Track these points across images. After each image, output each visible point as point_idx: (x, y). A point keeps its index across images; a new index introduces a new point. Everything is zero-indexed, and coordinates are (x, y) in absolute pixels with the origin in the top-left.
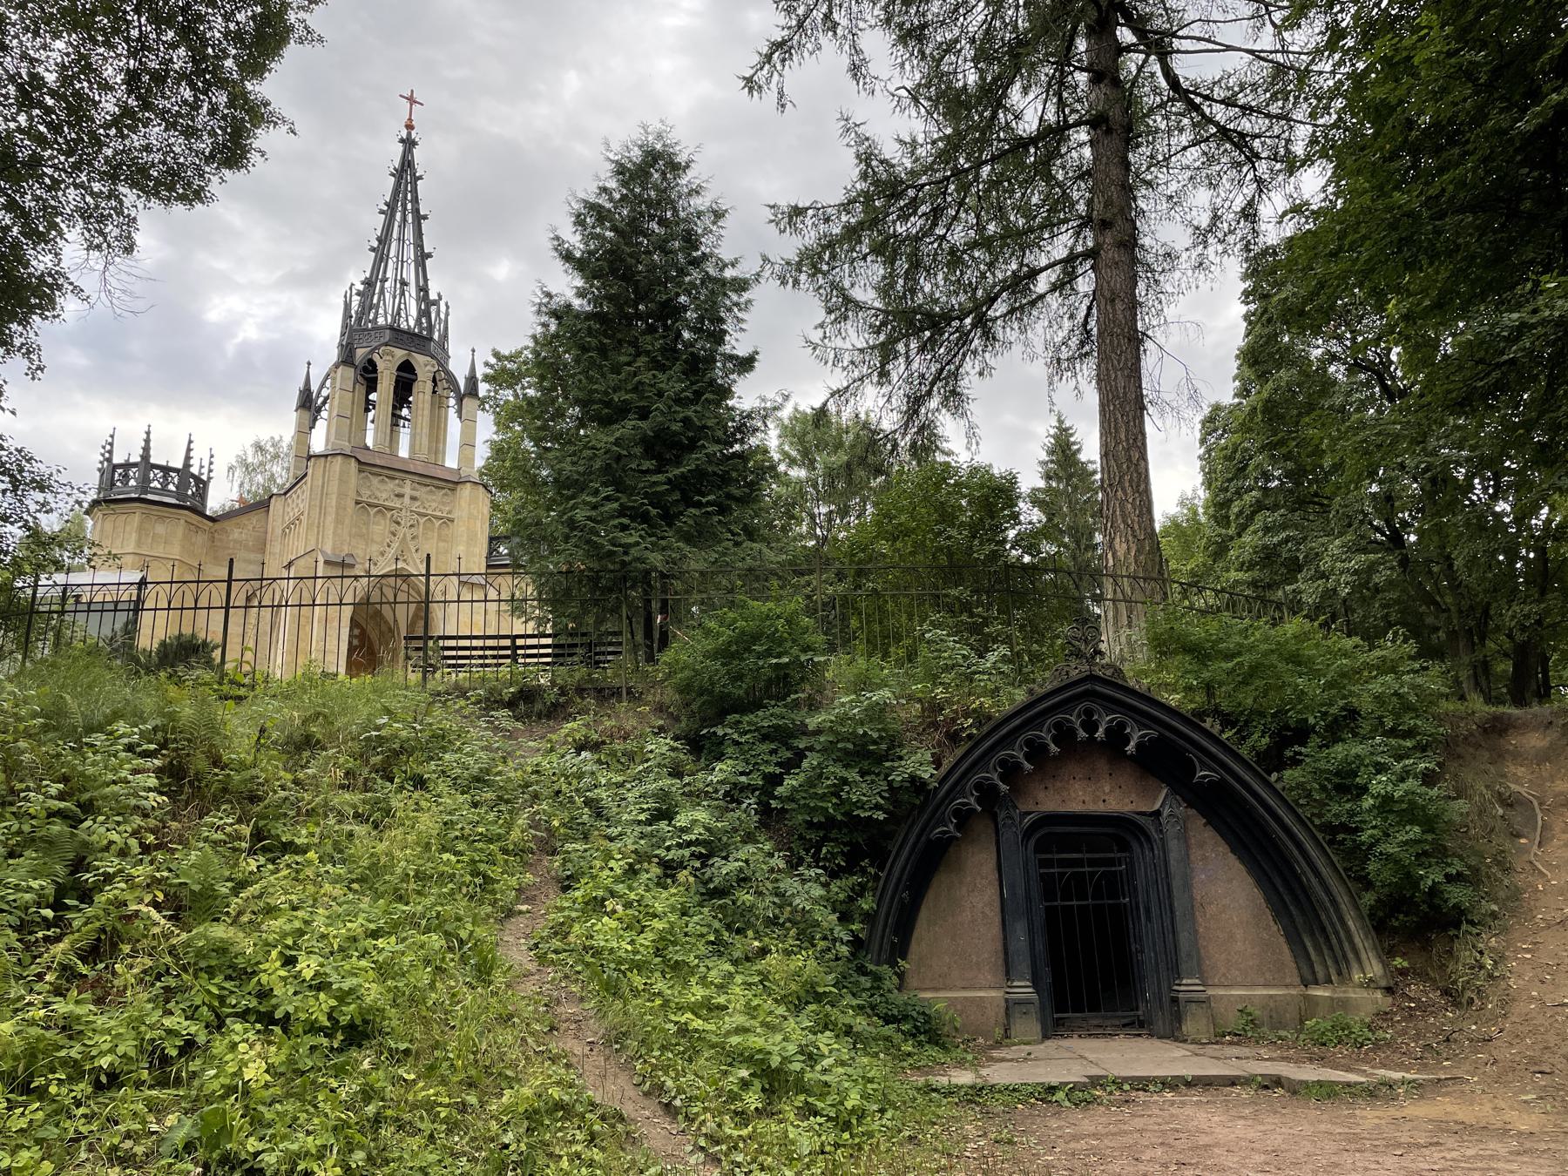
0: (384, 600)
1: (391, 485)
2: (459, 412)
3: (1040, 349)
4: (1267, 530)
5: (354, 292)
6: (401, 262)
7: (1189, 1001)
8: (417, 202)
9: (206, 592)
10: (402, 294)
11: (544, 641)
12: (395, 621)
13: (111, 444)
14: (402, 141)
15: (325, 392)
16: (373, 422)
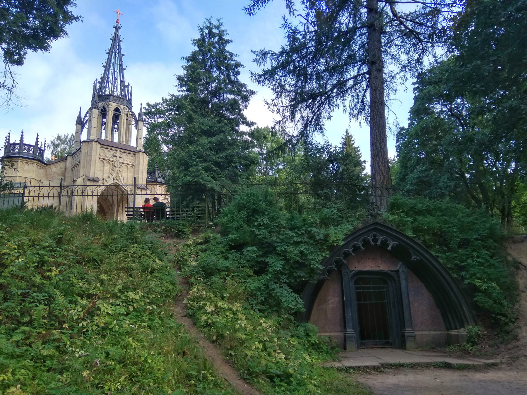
0: (109, 194)
1: (112, 152)
3: (348, 108)
4: (421, 171)
6: (114, 71)
7: (409, 336)
9: (33, 191)
10: (115, 83)
12: (113, 201)
13: (9, 137)
14: (114, 27)
15: (87, 118)
16: (104, 129)
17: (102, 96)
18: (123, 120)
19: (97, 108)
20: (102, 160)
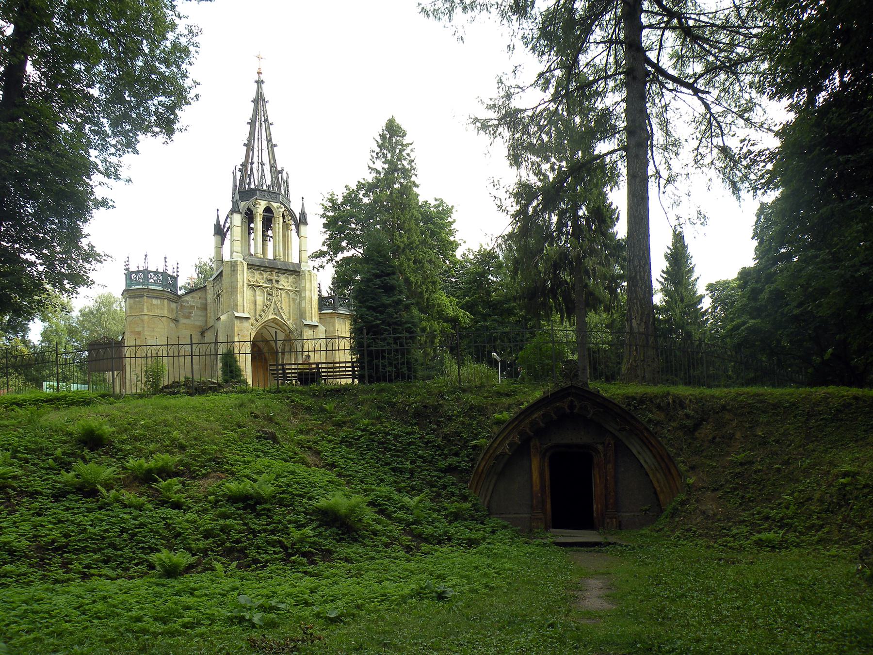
2: (298, 232)
5: (237, 169)
11: (348, 365)
15: (227, 225)
17: (246, 191)
18: (277, 225)
19: (239, 212)
20: (253, 287)
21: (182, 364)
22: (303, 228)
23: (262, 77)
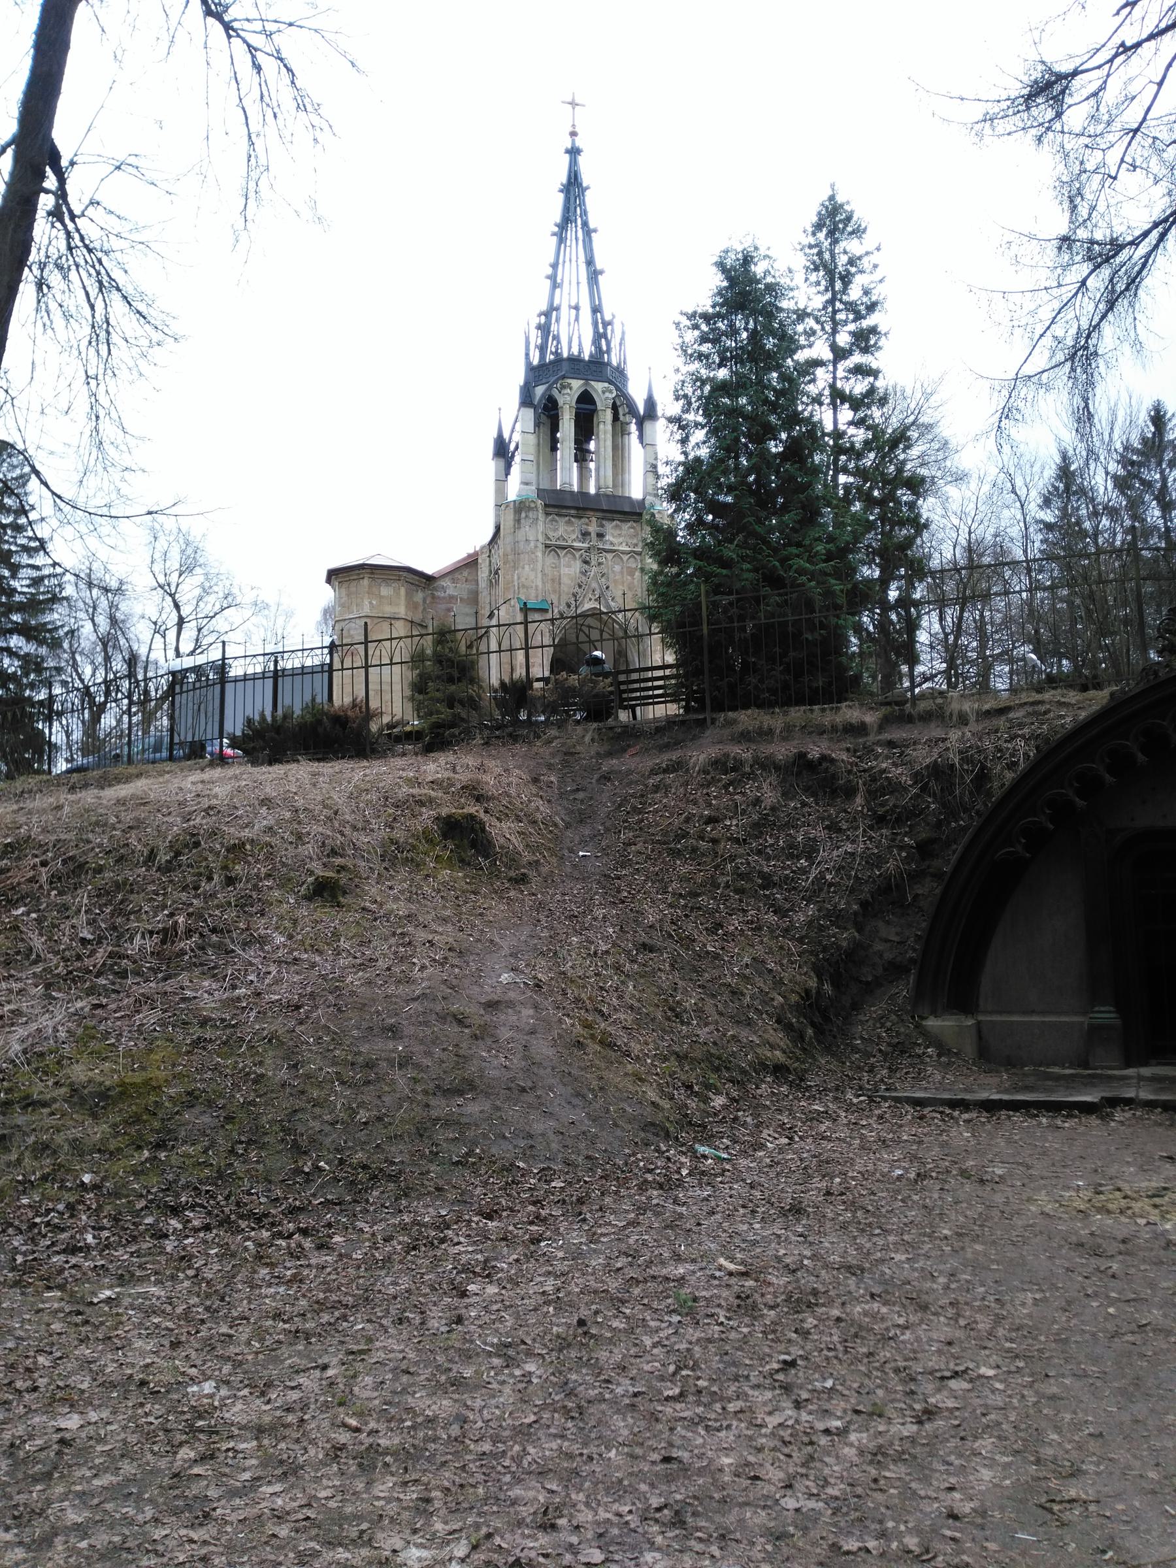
2: (641, 437)
8: (586, 214)
21: (184, 702)
22: (648, 425)
23: (579, 142)
